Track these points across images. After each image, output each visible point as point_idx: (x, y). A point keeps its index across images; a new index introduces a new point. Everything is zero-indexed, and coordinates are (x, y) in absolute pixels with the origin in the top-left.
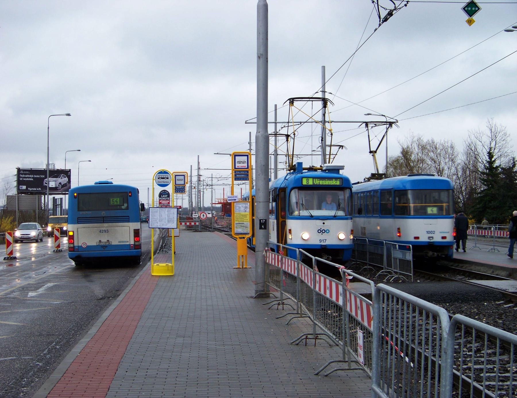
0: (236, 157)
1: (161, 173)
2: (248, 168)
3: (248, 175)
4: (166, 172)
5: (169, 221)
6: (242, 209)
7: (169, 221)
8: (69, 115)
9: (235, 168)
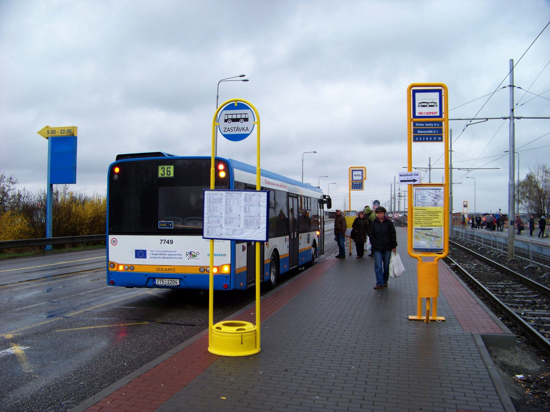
0: (417, 94)
1: (231, 107)
2: (441, 116)
3: (440, 131)
4: (242, 106)
5: (247, 224)
6: (429, 199)
7: (247, 224)
8: (315, 152)
9: (415, 116)
